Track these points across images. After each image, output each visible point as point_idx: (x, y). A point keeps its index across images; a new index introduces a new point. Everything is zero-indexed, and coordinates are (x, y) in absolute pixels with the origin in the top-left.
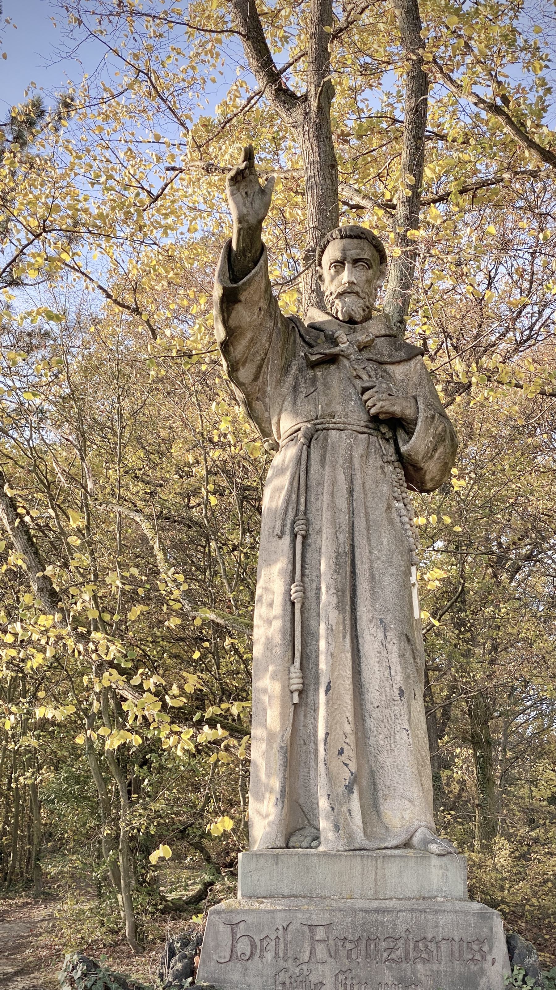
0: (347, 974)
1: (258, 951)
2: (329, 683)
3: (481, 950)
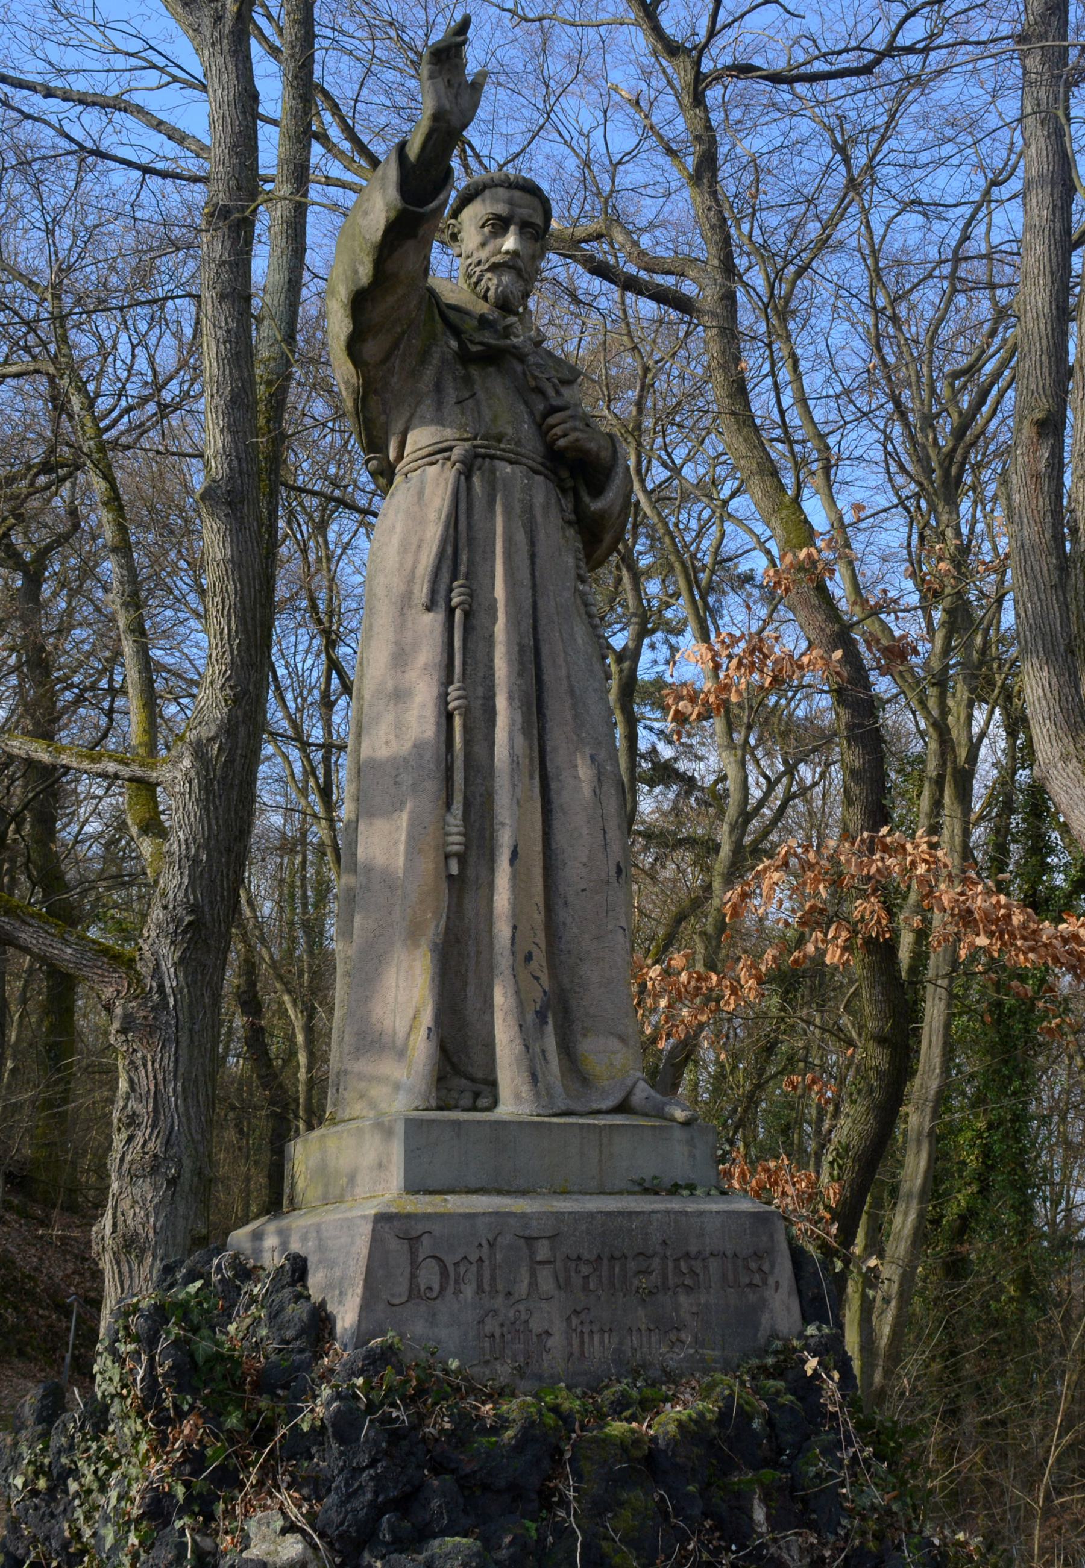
0: (583, 1316)
1: (452, 1282)
2: (516, 847)
3: (760, 1269)
